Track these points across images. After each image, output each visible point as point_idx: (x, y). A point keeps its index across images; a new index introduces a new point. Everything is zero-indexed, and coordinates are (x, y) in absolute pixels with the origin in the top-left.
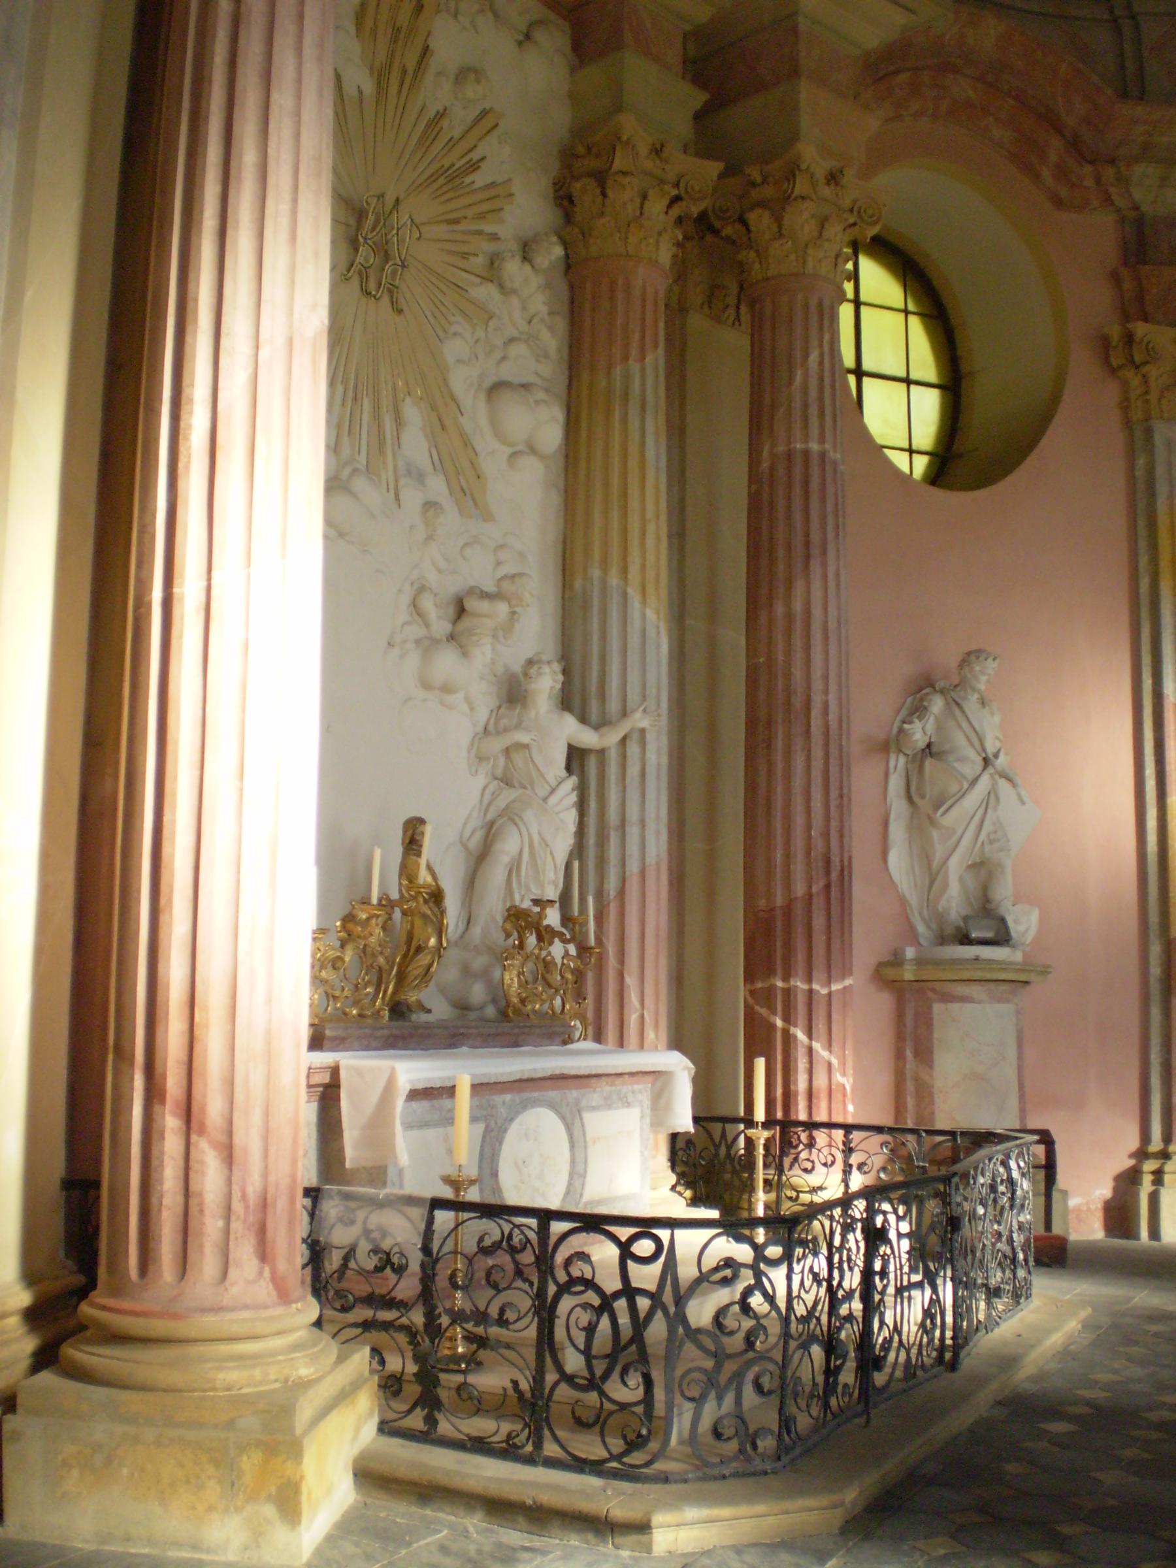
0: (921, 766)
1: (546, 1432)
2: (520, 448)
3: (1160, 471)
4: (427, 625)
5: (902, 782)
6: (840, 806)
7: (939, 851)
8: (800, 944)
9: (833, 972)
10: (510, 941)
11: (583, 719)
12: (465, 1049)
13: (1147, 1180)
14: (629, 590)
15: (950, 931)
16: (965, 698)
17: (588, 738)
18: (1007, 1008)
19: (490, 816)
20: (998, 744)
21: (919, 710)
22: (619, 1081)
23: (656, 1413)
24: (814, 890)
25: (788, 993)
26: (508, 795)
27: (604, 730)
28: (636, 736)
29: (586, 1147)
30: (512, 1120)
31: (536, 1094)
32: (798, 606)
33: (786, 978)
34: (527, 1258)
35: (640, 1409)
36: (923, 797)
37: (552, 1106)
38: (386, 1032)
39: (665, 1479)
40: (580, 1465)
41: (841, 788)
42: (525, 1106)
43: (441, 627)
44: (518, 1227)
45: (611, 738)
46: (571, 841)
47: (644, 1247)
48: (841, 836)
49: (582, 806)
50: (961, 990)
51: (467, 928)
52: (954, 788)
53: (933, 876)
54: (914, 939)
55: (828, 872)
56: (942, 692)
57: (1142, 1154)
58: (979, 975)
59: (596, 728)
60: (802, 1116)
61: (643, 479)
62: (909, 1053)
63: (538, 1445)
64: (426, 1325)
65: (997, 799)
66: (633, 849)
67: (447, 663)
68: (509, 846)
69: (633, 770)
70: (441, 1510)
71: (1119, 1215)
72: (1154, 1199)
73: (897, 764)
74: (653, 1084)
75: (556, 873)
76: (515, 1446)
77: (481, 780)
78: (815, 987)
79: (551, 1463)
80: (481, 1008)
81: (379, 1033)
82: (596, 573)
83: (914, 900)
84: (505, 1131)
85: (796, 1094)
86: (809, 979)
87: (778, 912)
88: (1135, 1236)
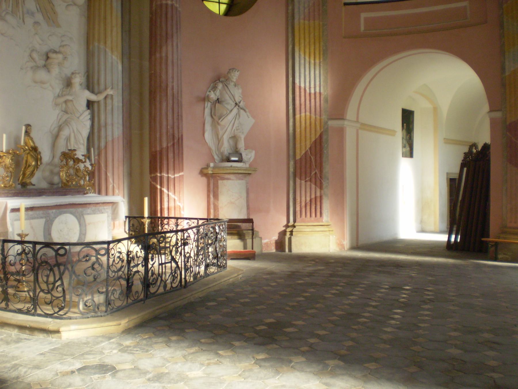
0: (215, 105)
1: (38, 307)
2: (70, 3)
3: (296, 11)
4: (35, 62)
5: (209, 111)
6: (178, 119)
7: (221, 133)
8: (165, 163)
9: (176, 171)
10: (63, 163)
11: (93, 92)
12: (44, 196)
13: (288, 234)
14: (107, 50)
15: (225, 158)
16: (229, 84)
17: (93, 97)
18: (243, 182)
19: (60, 123)
20: (241, 99)
21: (214, 88)
22: (98, 205)
23: (66, 300)
24: (169, 145)
25: (161, 178)
26: (66, 117)
27: (99, 95)
28: (110, 97)
29: (85, 226)
30: (56, 218)
31: (65, 210)
32: (164, 55)
33: (161, 173)
34: (30, 256)
35: (62, 299)
36: (215, 116)
37: (71, 213)
38: (13, 192)
39: (70, 318)
40: (47, 315)
41: (178, 113)
42: (61, 214)
43: (42, 62)
44: (27, 247)
45: (101, 97)
46: (88, 131)
47: (62, 252)
48: (178, 128)
49: (92, 119)
50: (227, 176)
51: (53, 159)
52: (225, 113)
53: (219, 140)
54: (213, 160)
55: (174, 140)
56: (222, 82)
57: (287, 226)
58: (232, 171)
59: (96, 94)
60: (166, 215)
61: (111, 13)
62: (211, 196)
63: (36, 311)
64: (4, 277)
65: (239, 116)
66: (109, 133)
67: (42, 75)
68: (65, 133)
69: (109, 108)
70: (6, 330)
71: (280, 245)
72: (290, 240)
73: (208, 105)
74: (112, 206)
75: (84, 141)
76: (29, 311)
77: (57, 111)
78: (170, 175)
79: (39, 315)
80: (58, 184)
81: (11, 192)
82: (96, 44)
83: (213, 148)
84: (53, 221)
85: (164, 209)
86: (168, 173)
87: (158, 153)
88: (285, 251)
